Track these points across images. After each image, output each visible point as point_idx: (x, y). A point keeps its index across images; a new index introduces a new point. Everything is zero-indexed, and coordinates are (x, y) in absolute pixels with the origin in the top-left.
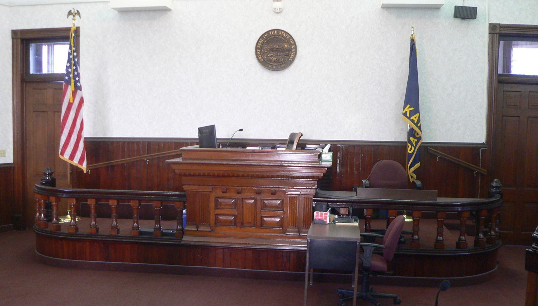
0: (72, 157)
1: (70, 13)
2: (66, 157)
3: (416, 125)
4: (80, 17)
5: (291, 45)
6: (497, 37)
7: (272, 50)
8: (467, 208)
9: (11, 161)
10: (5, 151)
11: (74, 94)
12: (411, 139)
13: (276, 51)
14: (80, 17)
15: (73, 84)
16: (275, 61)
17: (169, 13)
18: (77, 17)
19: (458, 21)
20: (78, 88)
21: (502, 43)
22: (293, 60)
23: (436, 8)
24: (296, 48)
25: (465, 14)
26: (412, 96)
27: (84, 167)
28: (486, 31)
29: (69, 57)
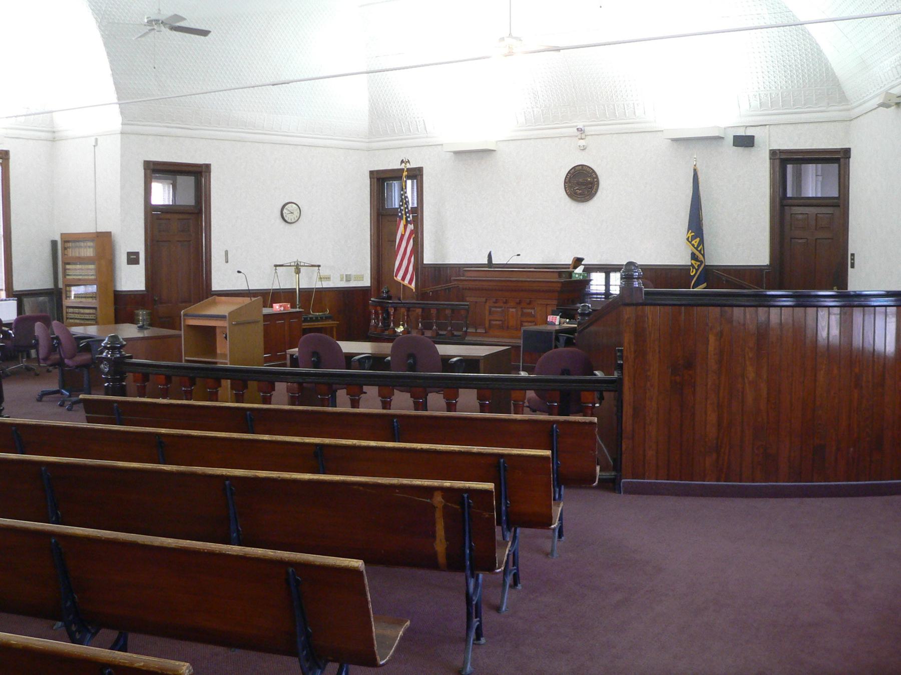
2: (399, 278)
6: (149, 171)
7: (578, 184)
9: (369, 284)
12: (693, 262)
13: (582, 184)
16: (580, 194)
19: (740, 149)
22: (596, 193)
23: (719, 138)
25: (745, 142)
27: (413, 286)
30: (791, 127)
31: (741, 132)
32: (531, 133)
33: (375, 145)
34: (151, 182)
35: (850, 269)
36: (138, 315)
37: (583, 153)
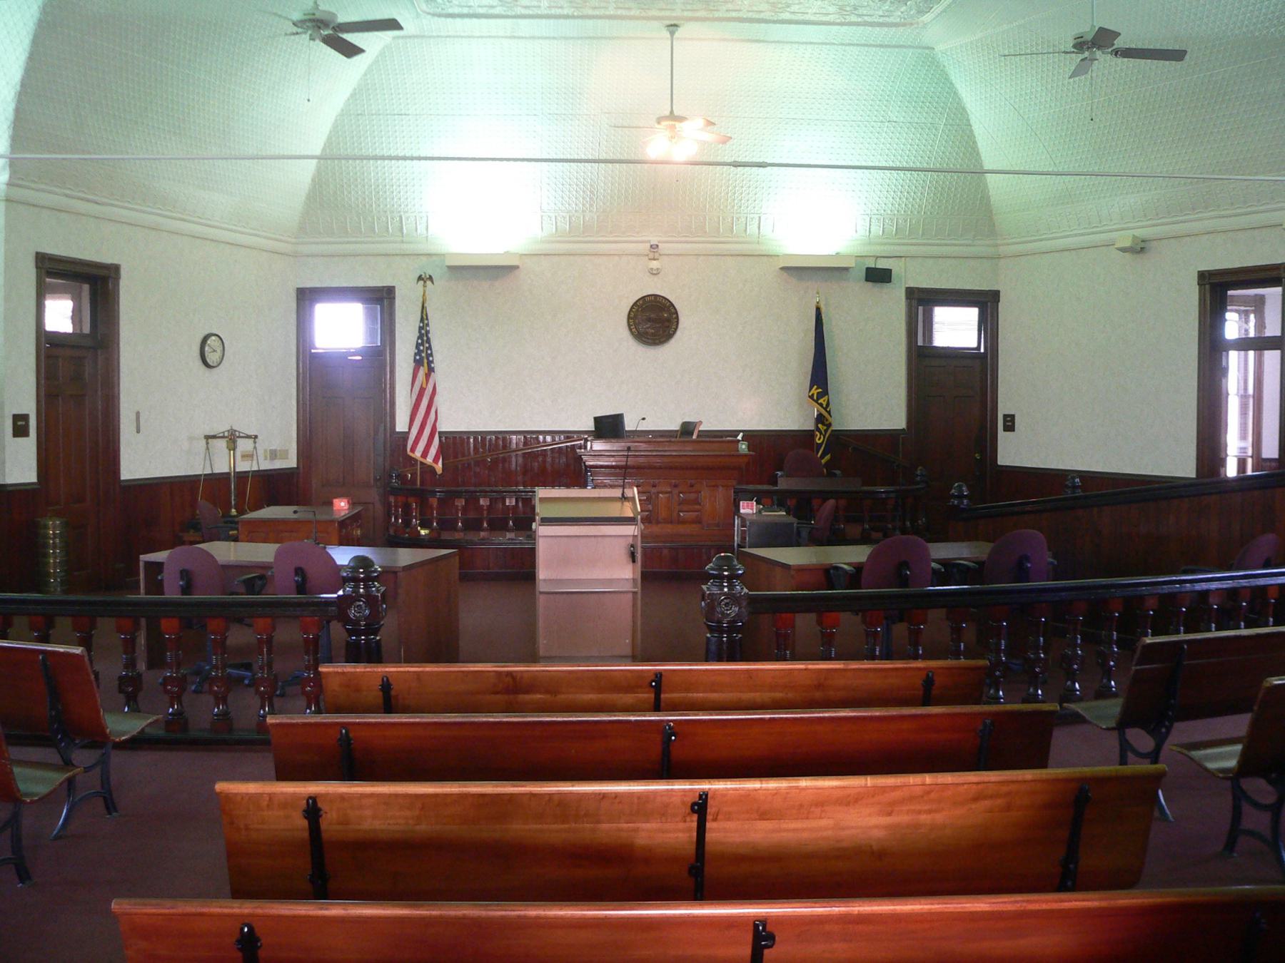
0: (425, 454)
1: (420, 278)
5: (671, 314)
6: (914, 303)
7: (649, 320)
8: (893, 495)
11: (428, 376)
17: (516, 272)
18: (429, 283)
19: (870, 284)
21: (921, 308)
22: (675, 332)
24: (677, 318)
25: (878, 276)
26: (819, 375)
27: (439, 467)
30: (931, 261)
31: (882, 264)
32: (904, 248)
35: (1001, 434)
36: (46, 527)
37: (656, 278)
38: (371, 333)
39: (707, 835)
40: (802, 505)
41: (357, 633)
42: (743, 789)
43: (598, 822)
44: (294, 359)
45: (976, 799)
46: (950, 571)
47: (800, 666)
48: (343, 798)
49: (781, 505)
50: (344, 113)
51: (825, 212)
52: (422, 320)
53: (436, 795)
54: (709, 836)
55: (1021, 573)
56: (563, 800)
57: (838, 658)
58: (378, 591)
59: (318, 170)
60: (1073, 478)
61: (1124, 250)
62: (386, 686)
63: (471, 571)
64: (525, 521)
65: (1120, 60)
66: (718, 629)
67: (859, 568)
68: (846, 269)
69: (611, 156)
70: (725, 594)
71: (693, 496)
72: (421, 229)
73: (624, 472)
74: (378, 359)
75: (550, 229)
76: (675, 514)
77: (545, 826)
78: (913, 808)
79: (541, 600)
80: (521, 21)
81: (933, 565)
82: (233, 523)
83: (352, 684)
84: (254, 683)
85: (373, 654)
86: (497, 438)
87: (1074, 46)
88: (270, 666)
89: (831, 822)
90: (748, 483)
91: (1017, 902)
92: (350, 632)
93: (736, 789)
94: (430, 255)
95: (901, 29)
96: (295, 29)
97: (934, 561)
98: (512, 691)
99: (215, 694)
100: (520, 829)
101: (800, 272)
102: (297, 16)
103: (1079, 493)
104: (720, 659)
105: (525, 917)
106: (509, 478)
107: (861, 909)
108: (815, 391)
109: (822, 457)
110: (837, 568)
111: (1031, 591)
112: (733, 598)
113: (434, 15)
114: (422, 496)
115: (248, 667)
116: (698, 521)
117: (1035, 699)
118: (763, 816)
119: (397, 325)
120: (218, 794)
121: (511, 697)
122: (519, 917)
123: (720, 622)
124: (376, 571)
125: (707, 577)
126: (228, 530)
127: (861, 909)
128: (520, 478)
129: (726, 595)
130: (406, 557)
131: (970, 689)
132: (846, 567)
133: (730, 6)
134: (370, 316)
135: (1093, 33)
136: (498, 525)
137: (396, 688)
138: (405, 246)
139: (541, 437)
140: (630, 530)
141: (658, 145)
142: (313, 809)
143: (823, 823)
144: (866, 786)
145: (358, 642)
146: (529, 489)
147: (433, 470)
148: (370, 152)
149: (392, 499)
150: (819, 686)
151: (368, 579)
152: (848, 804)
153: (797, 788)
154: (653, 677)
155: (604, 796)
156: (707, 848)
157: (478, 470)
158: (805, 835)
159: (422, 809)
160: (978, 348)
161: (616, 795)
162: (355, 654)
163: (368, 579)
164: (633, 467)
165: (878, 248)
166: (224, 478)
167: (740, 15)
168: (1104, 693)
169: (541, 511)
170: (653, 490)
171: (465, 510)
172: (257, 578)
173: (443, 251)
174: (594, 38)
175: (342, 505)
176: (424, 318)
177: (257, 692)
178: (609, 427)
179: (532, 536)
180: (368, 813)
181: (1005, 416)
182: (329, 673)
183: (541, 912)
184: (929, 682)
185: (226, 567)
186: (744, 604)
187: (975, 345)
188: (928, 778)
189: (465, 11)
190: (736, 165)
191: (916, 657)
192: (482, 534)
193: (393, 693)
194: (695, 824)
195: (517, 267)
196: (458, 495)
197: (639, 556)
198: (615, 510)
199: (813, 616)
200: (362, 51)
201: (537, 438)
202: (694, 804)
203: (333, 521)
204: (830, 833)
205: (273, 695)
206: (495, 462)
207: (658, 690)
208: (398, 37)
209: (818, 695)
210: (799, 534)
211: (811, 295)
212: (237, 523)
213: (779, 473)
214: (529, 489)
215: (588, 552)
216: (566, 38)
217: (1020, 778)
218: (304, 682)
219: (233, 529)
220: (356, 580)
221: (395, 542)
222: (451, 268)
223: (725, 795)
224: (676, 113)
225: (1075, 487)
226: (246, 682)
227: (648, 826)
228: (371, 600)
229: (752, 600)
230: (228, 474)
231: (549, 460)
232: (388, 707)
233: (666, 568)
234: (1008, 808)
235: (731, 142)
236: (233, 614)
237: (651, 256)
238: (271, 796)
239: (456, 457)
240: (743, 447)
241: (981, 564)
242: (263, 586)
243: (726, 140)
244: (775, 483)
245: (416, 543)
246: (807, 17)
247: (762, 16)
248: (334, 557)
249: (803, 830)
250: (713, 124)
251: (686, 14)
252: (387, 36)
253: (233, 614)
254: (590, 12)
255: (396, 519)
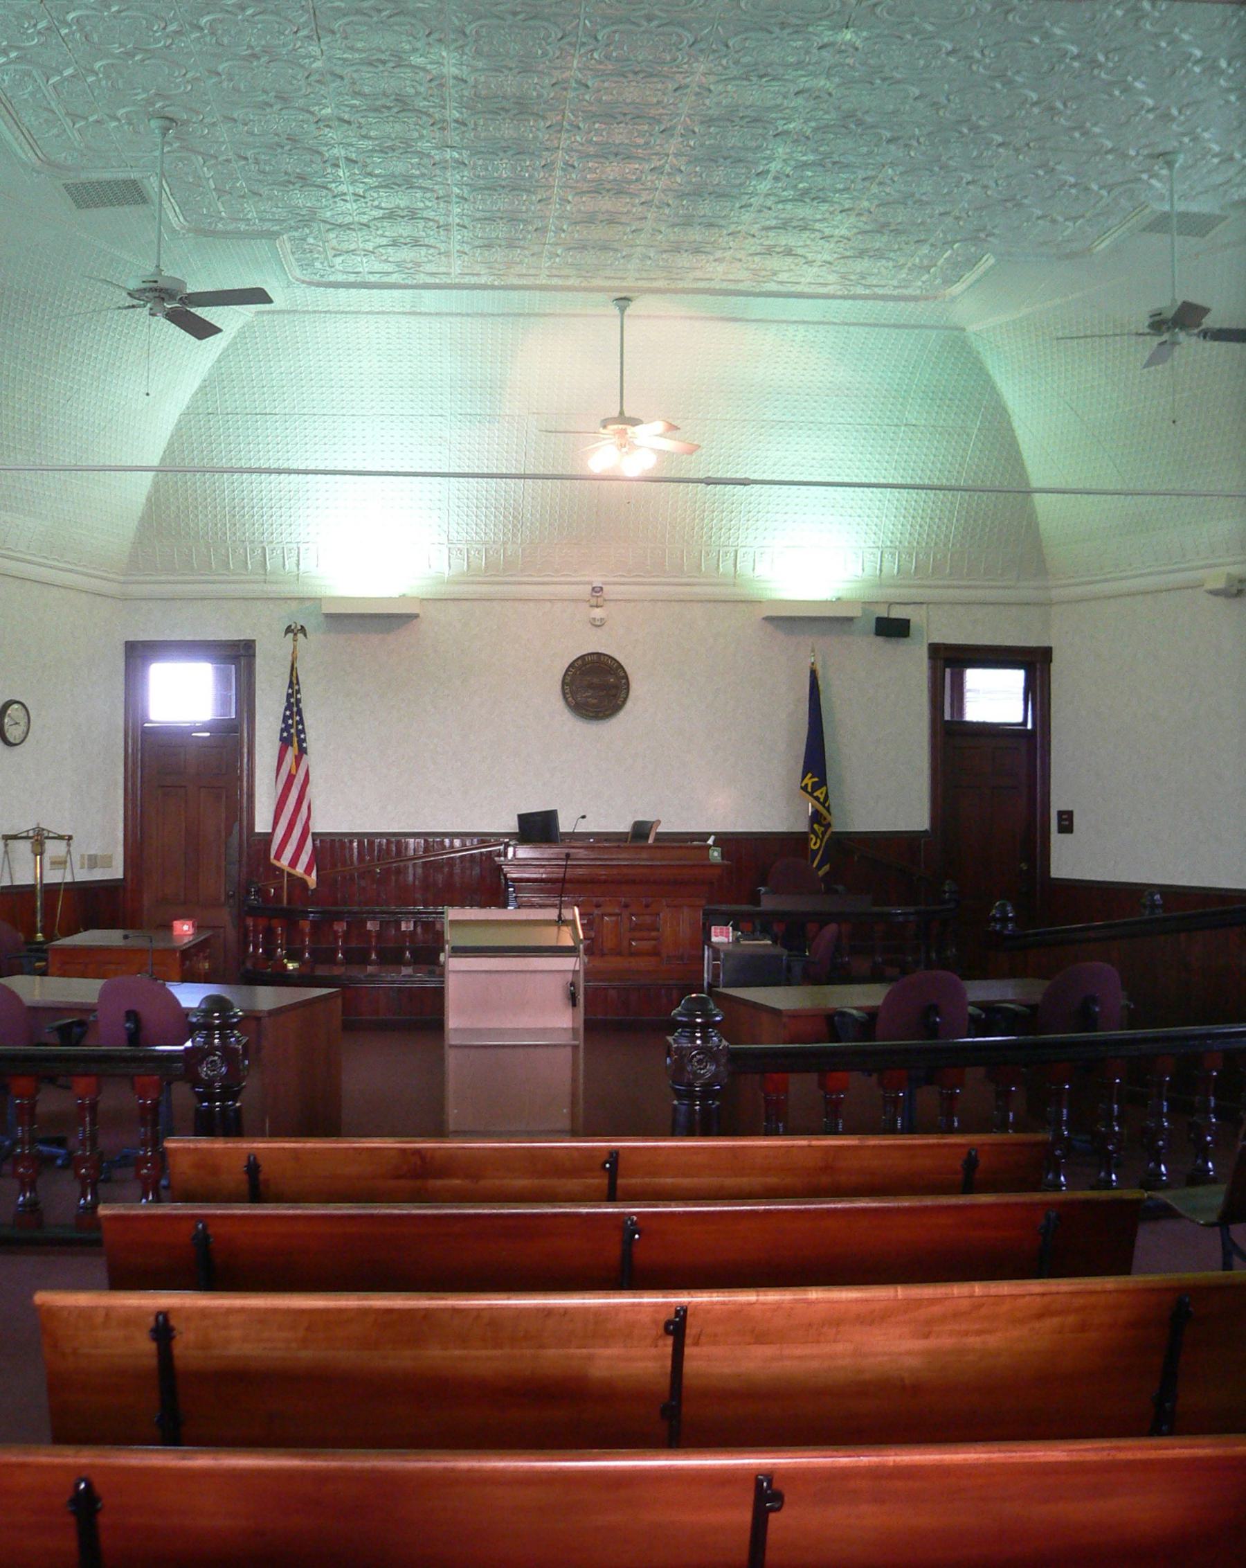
0: (294, 862)
1: (289, 630)
3: (823, 804)
4: (305, 635)
6: (940, 663)
7: (591, 686)
8: (911, 918)
9: (119, 874)
10: (110, 857)
11: (298, 759)
12: (816, 826)
14: (305, 635)
15: (296, 744)
18: (300, 636)
19: (880, 639)
20: (302, 751)
24: (628, 684)
25: (892, 629)
26: (815, 760)
27: (312, 880)
28: (924, 653)
29: (288, 700)
31: (897, 613)
33: (134, 590)
34: (208, 658)
35: (1055, 837)
38: (223, 702)
39: (685, 1363)
40: (792, 931)
41: (211, 1098)
42: (734, 1303)
43: (542, 1347)
44: (121, 735)
45: (1040, 1316)
46: (991, 1018)
47: (802, 1142)
48: (204, 1313)
49: (765, 931)
50: (190, 413)
51: (819, 548)
52: (291, 686)
53: (327, 1311)
54: (689, 1366)
55: (1087, 1020)
56: (494, 1319)
57: (848, 1131)
58: (238, 1042)
59: (156, 484)
60: (1152, 895)
61: (1215, 593)
62: (253, 1168)
63: (357, 1019)
64: (428, 951)
65: (1209, 344)
66: (690, 1095)
67: (872, 1014)
68: (850, 620)
69: (541, 470)
70: (697, 1047)
71: (648, 919)
72: (290, 564)
73: (558, 887)
74: (231, 739)
75: (460, 565)
76: (625, 943)
77: (474, 1353)
78: (957, 1327)
79: (452, 1058)
80: (424, 293)
81: (971, 1009)
82: (40, 951)
83: (206, 1163)
84: (72, 1162)
85: (232, 1127)
86: (389, 842)
87: (1152, 326)
88: (93, 1139)
89: (849, 1347)
90: (720, 903)
91: (1103, 1449)
92: (202, 1097)
93: (723, 1303)
94: (303, 599)
95: (922, 304)
96: (130, 301)
97: (972, 1004)
98: (419, 1175)
99: (21, 1177)
100: (438, 1356)
101: (794, 623)
102: (134, 284)
103: (1160, 913)
104: (690, 1133)
105: (453, 1470)
106: (405, 896)
107: (898, 1459)
108: (809, 781)
109: (819, 867)
110: (842, 1014)
111: (1105, 1043)
112: (708, 1054)
113: (310, 284)
114: (290, 918)
115: (61, 1142)
116: (655, 953)
117: (1108, 1184)
118: (761, 1338)
119: (258, 693)
120: (38, 1309)
121: (419, 1183)
122: (445, 1469)
123: (691, 1085)
124: (235, 1016)
125: (673, 1026)
126: (35, 960)
127: (898, 1459)
128: (418, 896)
129: (699, 1048)
130: (267, 998)
131: (1028, 1172)
132: (854, 1012)
133: (699, 274)
134: (223, 680)
135: (1176, 309)
136: (392, 958)
137: (266, 1169)
138: (268, 587)
139: (447, 841)
140: (569, 964)
141: (605, 457)
142: (163, 1329)
143: (839, 1347)
144: (895, 1299)
145: (210, 1109)
146: (431, 909)
147: (303, 883)
148: (224, 463)
149: (250, 922)
150: (827, 1168)
151: (226, 1026)
152: (872, 1323)
153: (806, 1301)
154: (606, 1157)
155: (548, 1312)
156: (685, 1382)
157: (363, 883)
158: (815, 1364)
159: (308, 1329)
160: (1025, 723)
161: (566, 1312)
162: (206, 1126)
163: (226, 1026)
164: (571, 881)
165: (892, 591)
166: (25, 893)
167: (712, 285)
168: (1198, 1178)
169: (452, 937)
170: (596, 911)
171: (346, 936)
172: (74, 1024)
173: (319, 595)
174: (520, 315)
175: (184, 929)
176: (294, 683)
177: (77, 1175)
178: (537, 828)
179: (439, 972)
180: (236, 1333)
181: (1060, 813)
182: (176, 1150)
183: (501, 1464)
184: (971, 1163)
185: (36, 1010)
186: (723, 1060)
187: (1020, 719)
188: (978, 1288)
189: (352, 278)
190: (709, 482)
191: (950, 1130)
192: (370, 969)
193: (261, 1177)
194: (669, 1350)
195: (416, 616)
196: (338, 916)
197: (581, 998)
198: (549, 937)
199: (814, 1077)
200: (218, 330)
201: (442, 842)
202: (668, 1323)
203: (174, 950)
204: (846, 1362)
205: (100, 1178)
206: (387, 872)
207: (613, 1174)
208: (263, 313)
209: (825, 1180)
210: (789, 969)
211: (797, 657)
212: (45, 951)
213: (763, 889)
214: (431, 909)
215: (513, 997)
216: (482, 315)
217: (1099, 1288)
218: (140, 1162)
219: (40, 960)
220: (209, 1028)
221: (253, 978)
222: (330, 616)
223: (708, 1312)
224: (627, 414)
225: (1154, 906)
226: (59, 1162)
227: (608, 1352)
228: (228, 1054)
229: (733, 1056)
230: (34, 886)
231: (457, 870)
232: (256, 1193)
233: (618, 1012)
234: (1083, 1327)
235: (699, 452)
236: (45, 1071)
237: (593, 602)
238: (108, 1311)
239: (334, 866)
240: (715, 854)
241: (1034, 1008)
242: (83, 1035)
243: (693, 449)
244: (758, 903)
245: (281, 979)
246: (799, 288)
247: (741, 286)
248: (178, 996)
249: (813, 1357)
250: (676, 428)
251: (641, 283)
252: (248, 311)
253: (45, 1071)
254: (516, 281)
255: (256, 948)
